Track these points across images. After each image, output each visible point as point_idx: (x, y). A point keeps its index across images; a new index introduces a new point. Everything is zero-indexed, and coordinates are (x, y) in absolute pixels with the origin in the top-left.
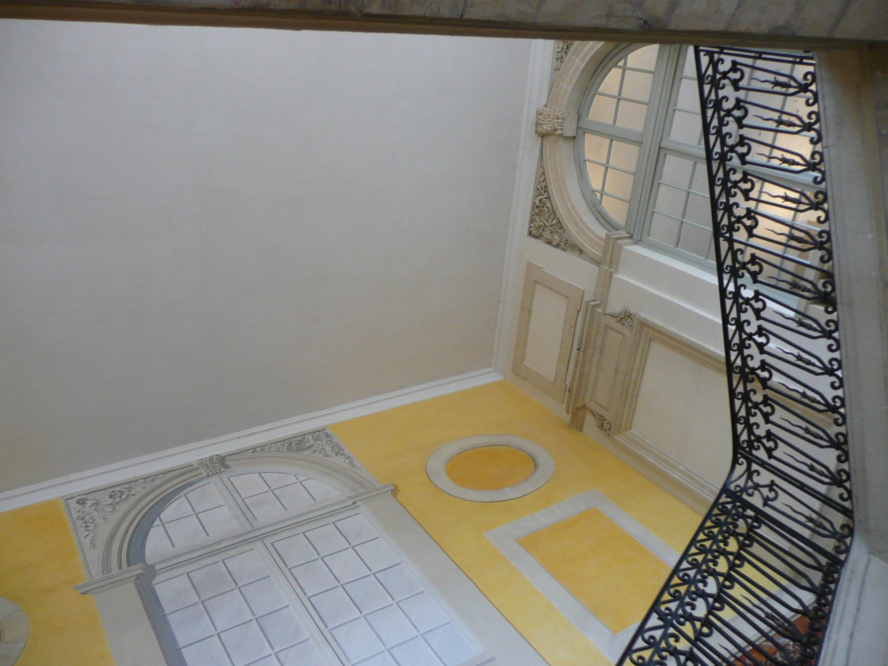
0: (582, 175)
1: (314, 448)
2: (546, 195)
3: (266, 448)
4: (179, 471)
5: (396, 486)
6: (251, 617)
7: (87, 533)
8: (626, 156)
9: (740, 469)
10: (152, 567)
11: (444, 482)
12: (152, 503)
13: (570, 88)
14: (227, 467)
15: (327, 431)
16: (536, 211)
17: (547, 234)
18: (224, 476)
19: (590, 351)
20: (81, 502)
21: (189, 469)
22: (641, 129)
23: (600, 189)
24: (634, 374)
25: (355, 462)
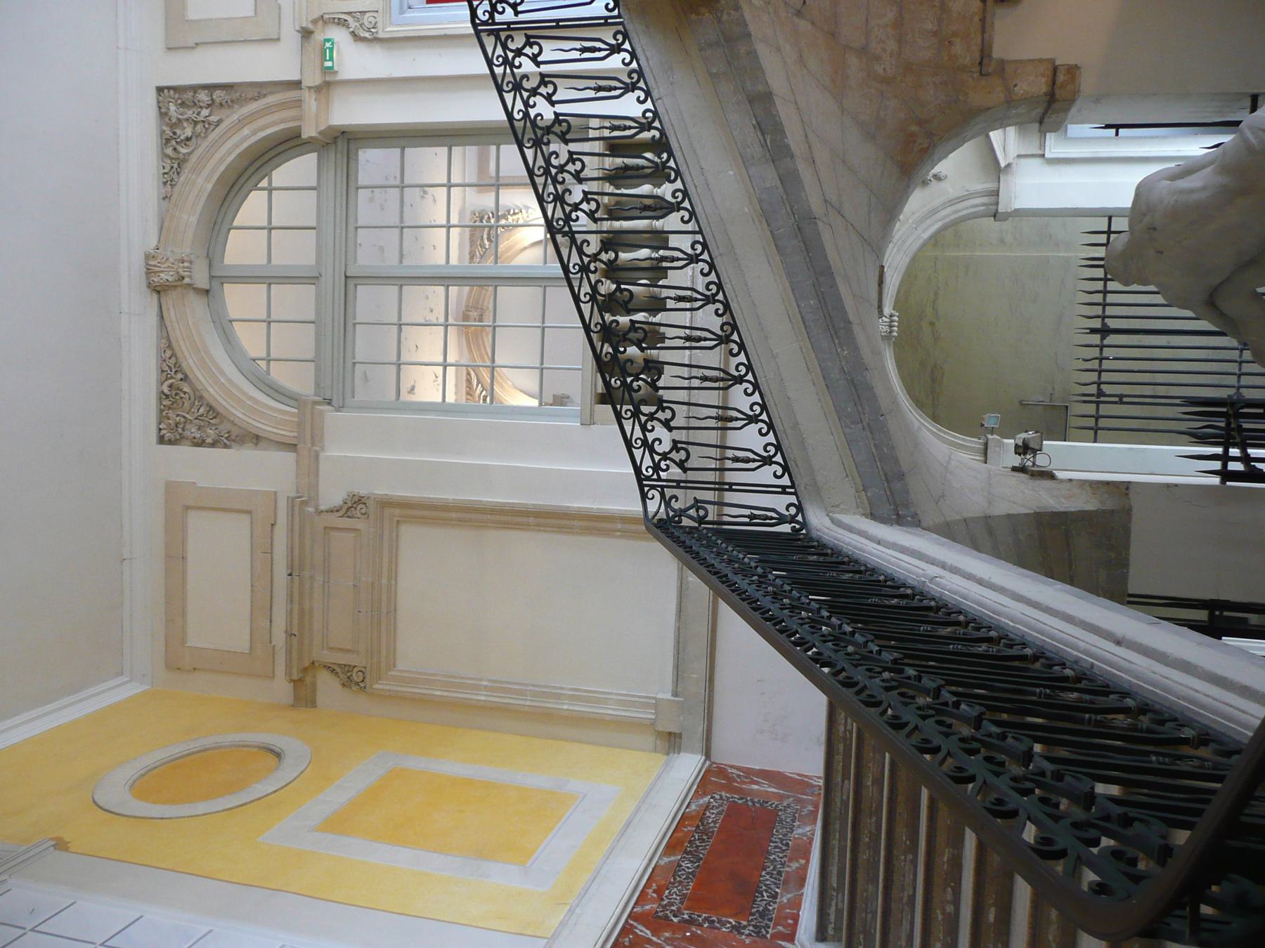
0: (229, 340)
2: (180, 376)
8: (296, 301)
13: (194, 220)
16: (166, 402)
17: (192, 431)
22: (313, 262)
23: (264, 355)
24: (384, 581)
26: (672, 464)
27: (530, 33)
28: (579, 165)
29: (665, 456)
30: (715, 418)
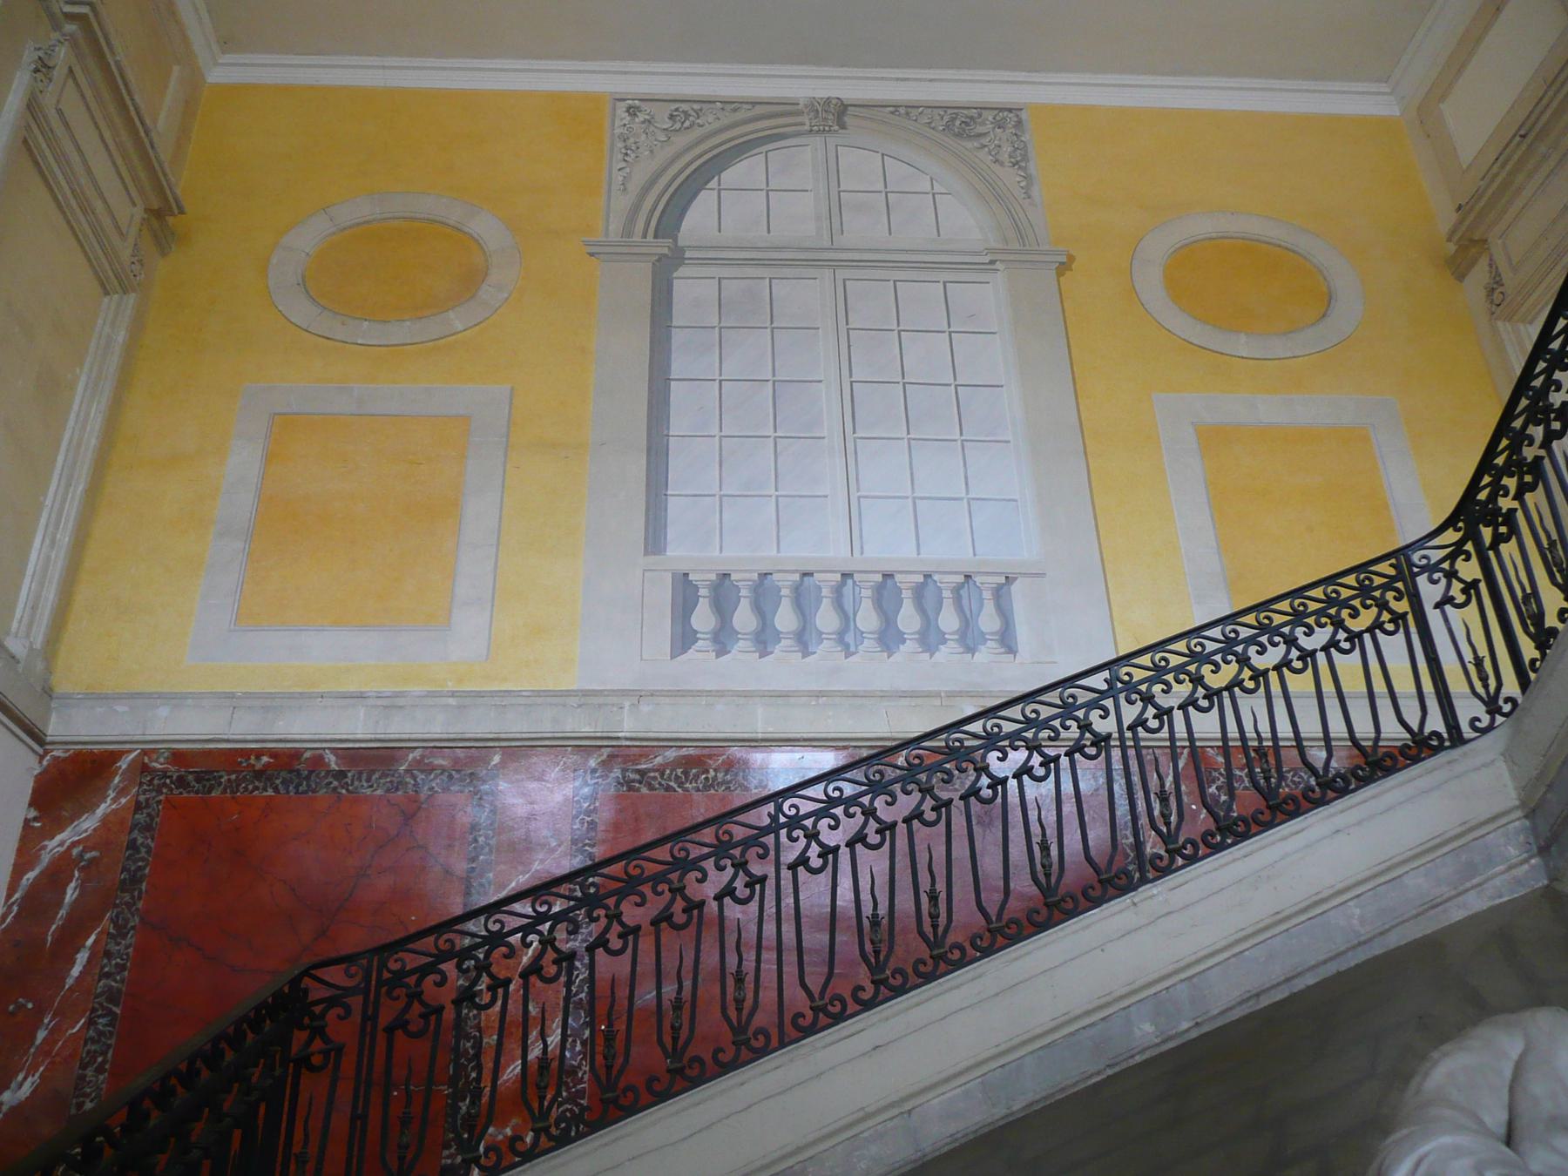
1: (985, 141)
3: (914, 112)
4: (781, 108)
5: (1071, 258)
6: (770, 377)
7: (623, 164)
9: (1451, 536)
10: (682, 250)
11: (1151, 284)
12: (731, 139)
14: (843, 126)
15: (1023, 115)
18: (832, 141)
19: (1543, 149)
20: (632, 111)
21: (785, 109)
25: (1035, 191)
26: (400, 1005)
27: (1483, 586)
28: (1040, 772)
29: (813, 836)
30: (875, 915)
